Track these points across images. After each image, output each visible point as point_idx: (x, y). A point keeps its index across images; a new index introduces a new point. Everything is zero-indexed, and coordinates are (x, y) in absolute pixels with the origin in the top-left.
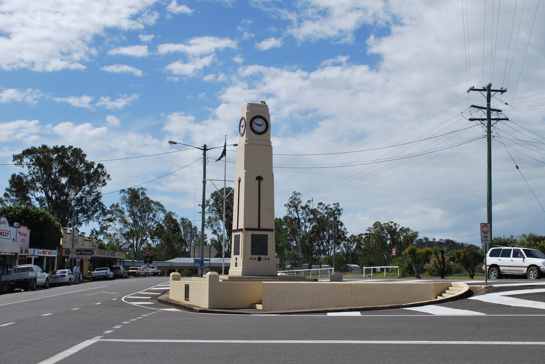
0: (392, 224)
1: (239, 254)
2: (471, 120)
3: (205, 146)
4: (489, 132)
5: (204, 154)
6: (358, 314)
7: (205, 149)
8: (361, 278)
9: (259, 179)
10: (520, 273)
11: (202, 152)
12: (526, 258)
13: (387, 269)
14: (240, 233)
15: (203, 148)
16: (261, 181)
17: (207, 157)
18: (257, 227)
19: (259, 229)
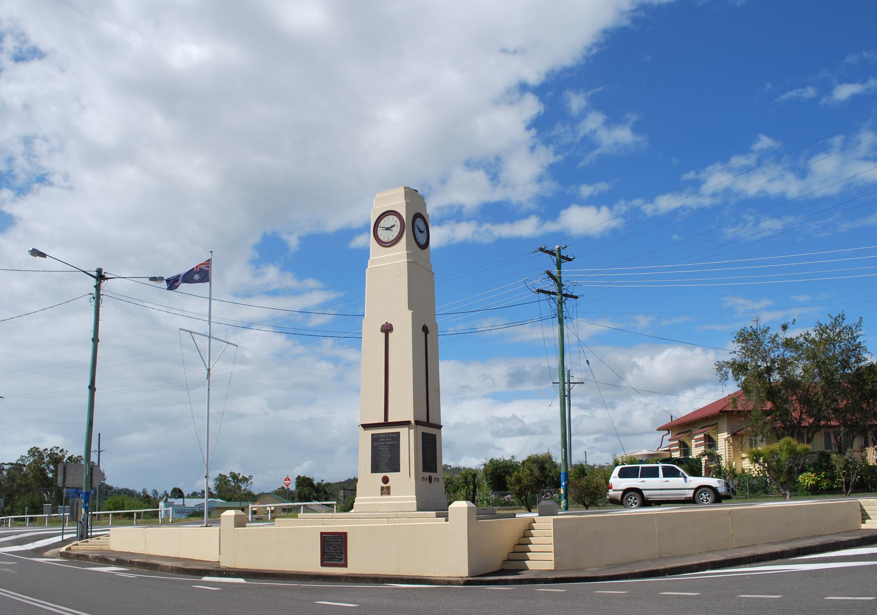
0: (58, 451)
1: (397, 470)
2: (539, 291)
3: (99, 271)
4: (561, 311)
5: (98, 287)
6: (241, 580)
7: (100, 277)
8: (785, 500)
9: (425, 329)
10: (683, 497)
11: (94, 282)
12: (689, 478)
13: (137, 513)
14: (403, 431)
15: (95, 274)
16: (390, 335)
17: (101, 292)
18: (381, 420)
19: (386, 424)
